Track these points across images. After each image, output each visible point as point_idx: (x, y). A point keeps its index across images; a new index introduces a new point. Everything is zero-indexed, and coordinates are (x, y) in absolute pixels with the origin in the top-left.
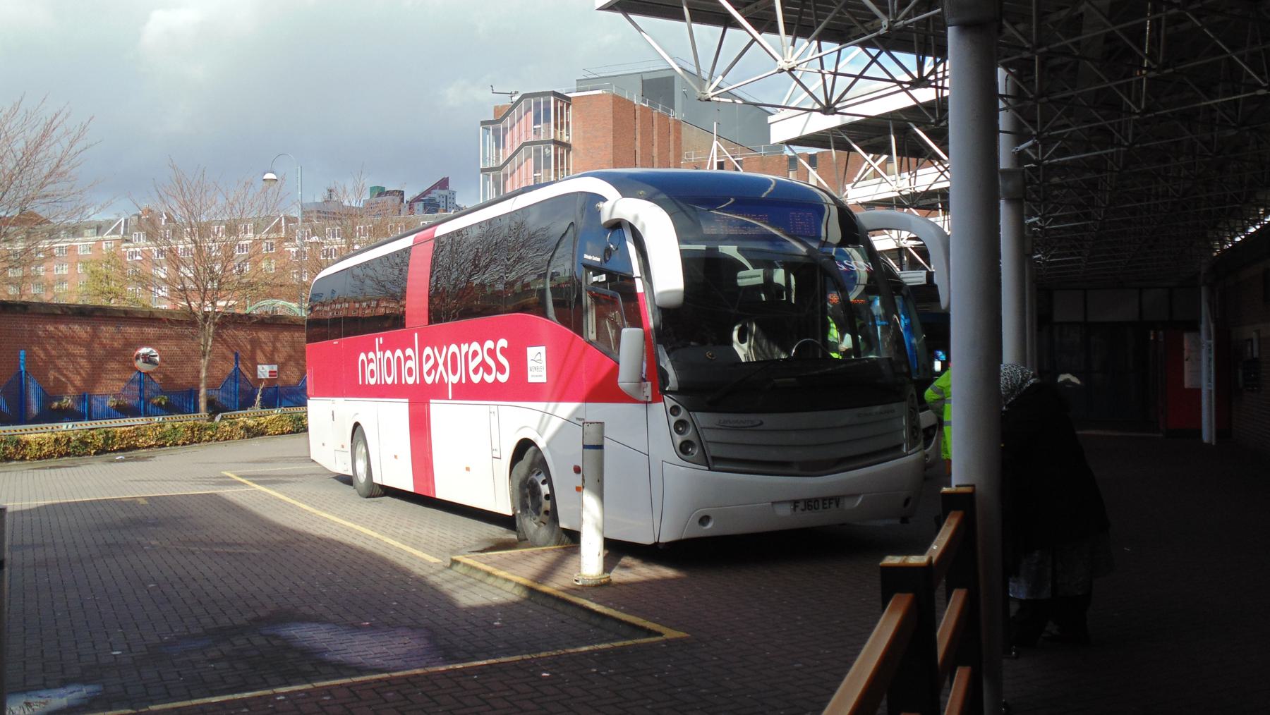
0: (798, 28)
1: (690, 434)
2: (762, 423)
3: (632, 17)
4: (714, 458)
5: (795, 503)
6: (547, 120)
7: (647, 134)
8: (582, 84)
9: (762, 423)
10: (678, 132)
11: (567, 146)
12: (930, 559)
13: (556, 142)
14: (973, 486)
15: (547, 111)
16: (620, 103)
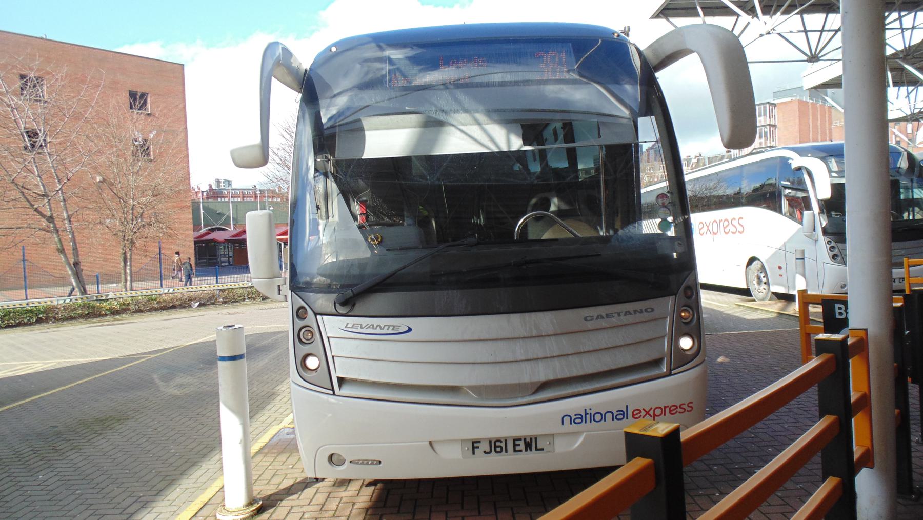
0: (768, 9)
1: (836, 252)
2: (410, 330)
3: (671, 19)
4: (341, 381)
5: (475, 444)
6: (765, 115)
7: (814, 115)
8: (776, 94)
9: (410, 330)
10: (830, 112)
11: (775, 126)
12: (676, 433)
13: (770, 125)
14: (866, 330)
15: (765, 111)
16: (801, 103)
